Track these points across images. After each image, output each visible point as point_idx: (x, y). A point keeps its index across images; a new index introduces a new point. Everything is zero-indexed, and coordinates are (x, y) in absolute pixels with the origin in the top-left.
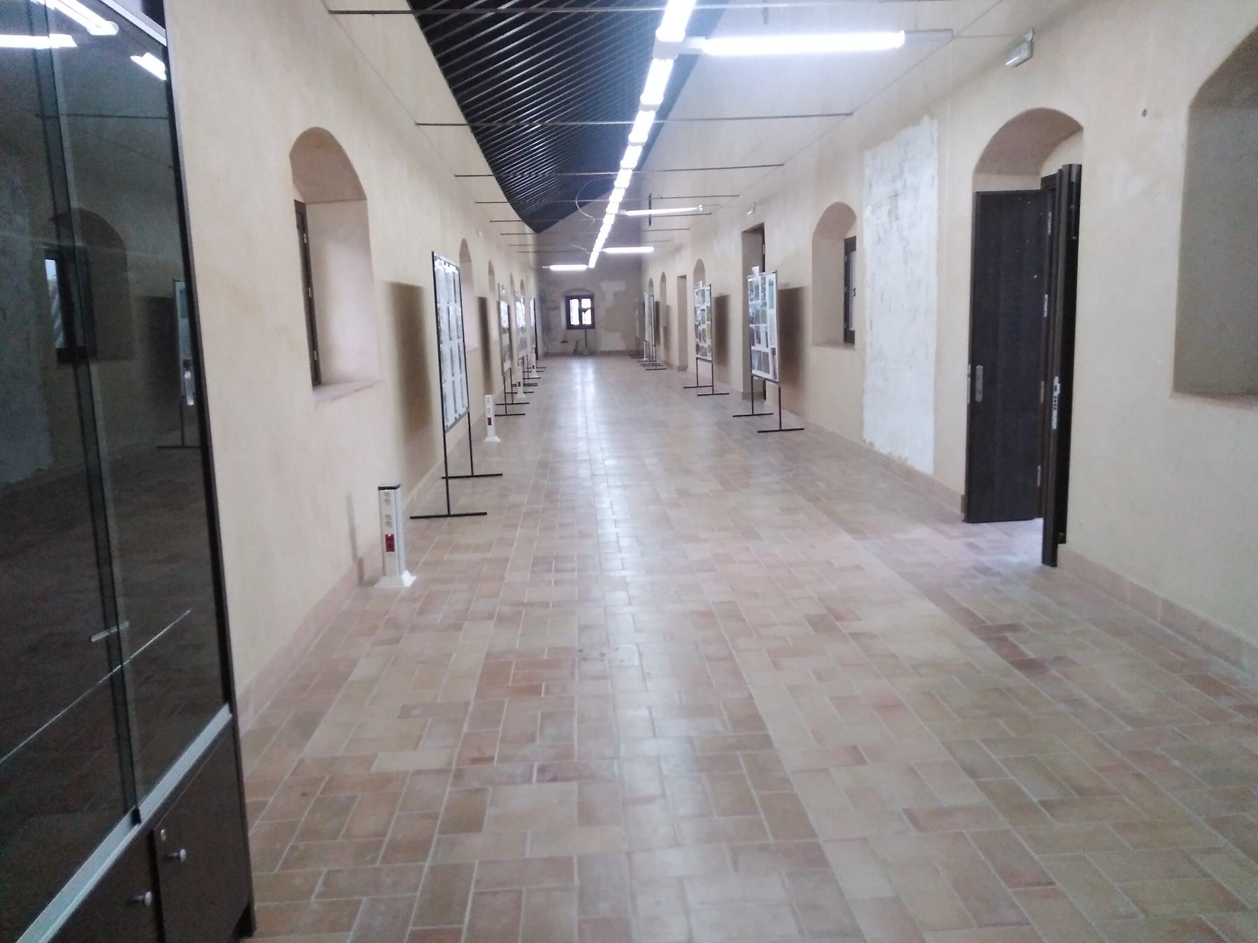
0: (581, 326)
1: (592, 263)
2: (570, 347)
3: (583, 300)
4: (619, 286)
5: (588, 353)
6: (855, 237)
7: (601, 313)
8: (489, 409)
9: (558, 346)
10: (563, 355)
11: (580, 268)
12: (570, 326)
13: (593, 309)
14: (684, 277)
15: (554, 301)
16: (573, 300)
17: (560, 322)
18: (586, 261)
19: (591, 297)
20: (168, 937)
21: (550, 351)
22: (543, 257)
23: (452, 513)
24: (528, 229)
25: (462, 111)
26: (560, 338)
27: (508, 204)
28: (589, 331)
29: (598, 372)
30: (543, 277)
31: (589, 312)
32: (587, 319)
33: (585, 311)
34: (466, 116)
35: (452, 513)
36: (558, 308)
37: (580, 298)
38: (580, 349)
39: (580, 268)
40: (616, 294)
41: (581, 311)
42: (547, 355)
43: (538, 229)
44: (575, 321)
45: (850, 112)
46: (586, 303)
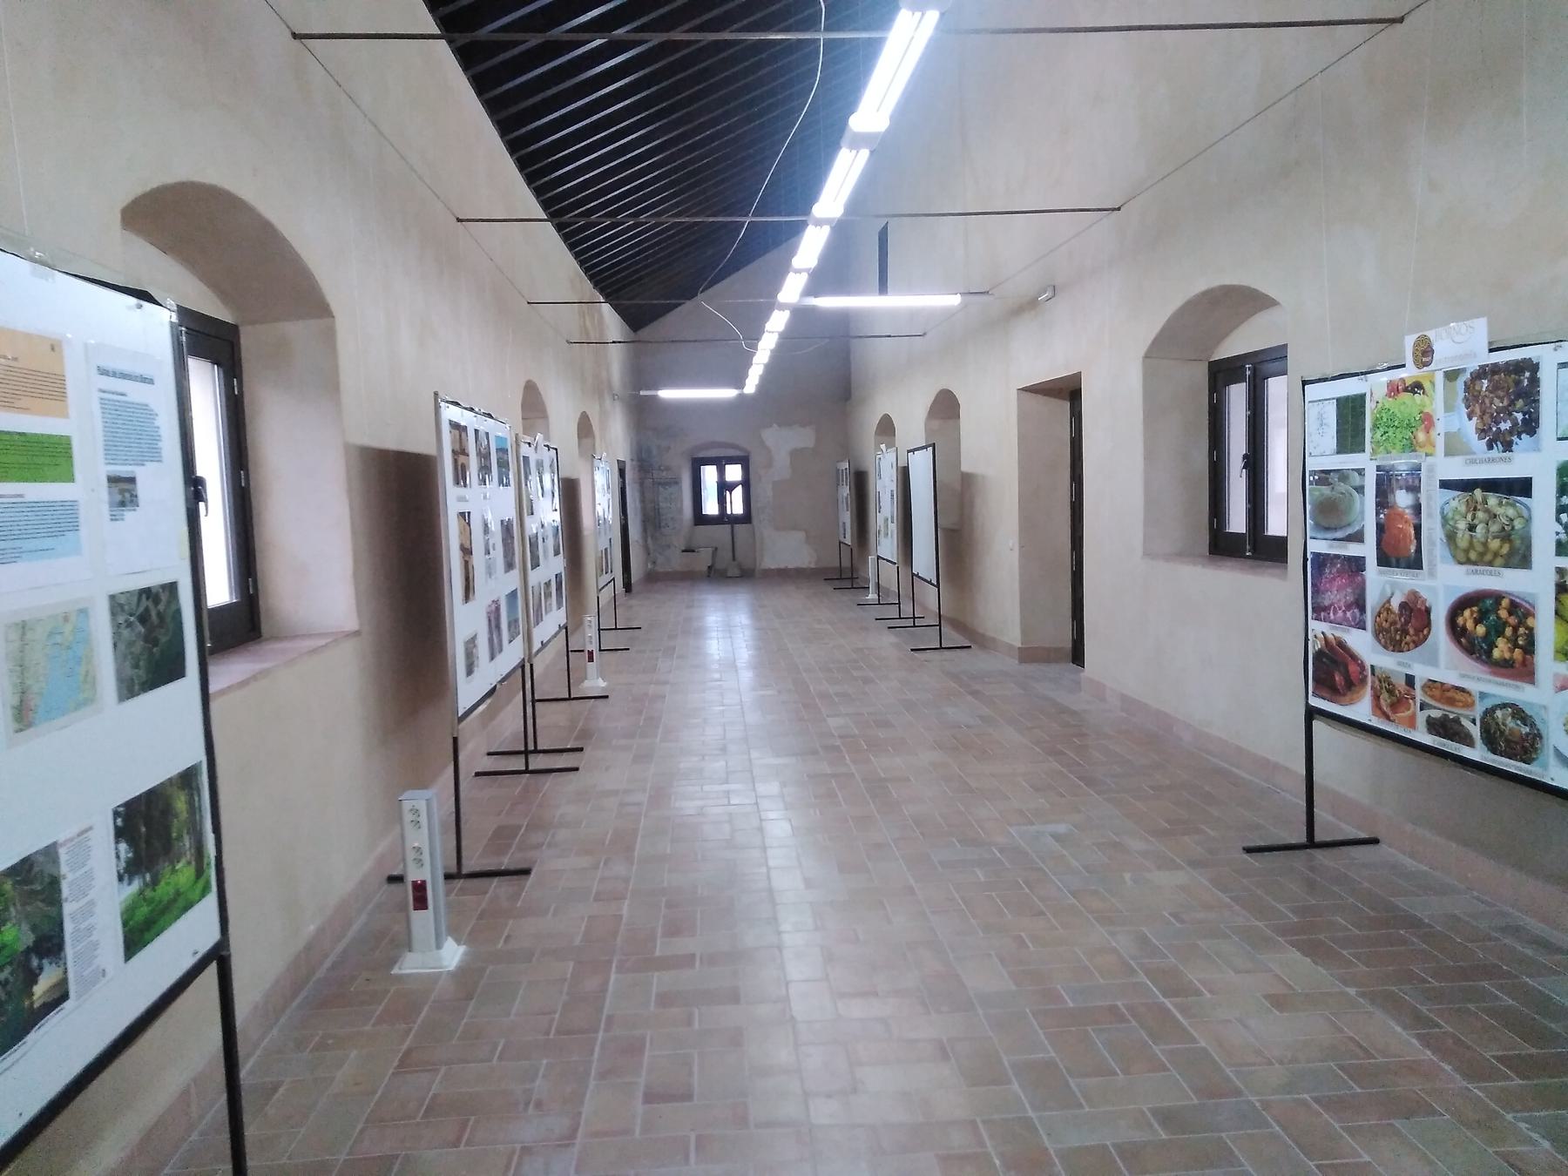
0: (723, 518)
1: (751, 386)
2: (702, 560)
3: (728, 468)
4: (803, 438)
5: (736, 572)
6: (1285, 346)
7: (763, 491)
8: (418, 850)
9: (676, 561)
10: (688, 577)
11: (727, 393)
12: (700, 519)
13: (746, 483)
14: (1069, 392)
15: (668, 469)
16: (707, 467)
17: (680, 511)
18: (739, 382)
19: (744, 461)
20: (252, 1163)
21: (660, 569)
22: (642, 376)
23: (539, 748)
24: (610, 321)
25: (512, 154)
26: (680, 543)
27: (442, 44)
28: (739, 528)
29: (755, 614)
30: (643, 413)
31: (738, 492)
32: (736, 505)
33: (732, 487)
34: (546, 205)
35: (530, 768)
36: (676, 482)
37: (720, 463)
38: (718, 566)
39: (727, 393)
40: (795, 454)
41: (724, 487)
42: (652, 578)
43: (635, 319)
44: (711, 507)
45: (1398, 15)
46: (734, 473)
